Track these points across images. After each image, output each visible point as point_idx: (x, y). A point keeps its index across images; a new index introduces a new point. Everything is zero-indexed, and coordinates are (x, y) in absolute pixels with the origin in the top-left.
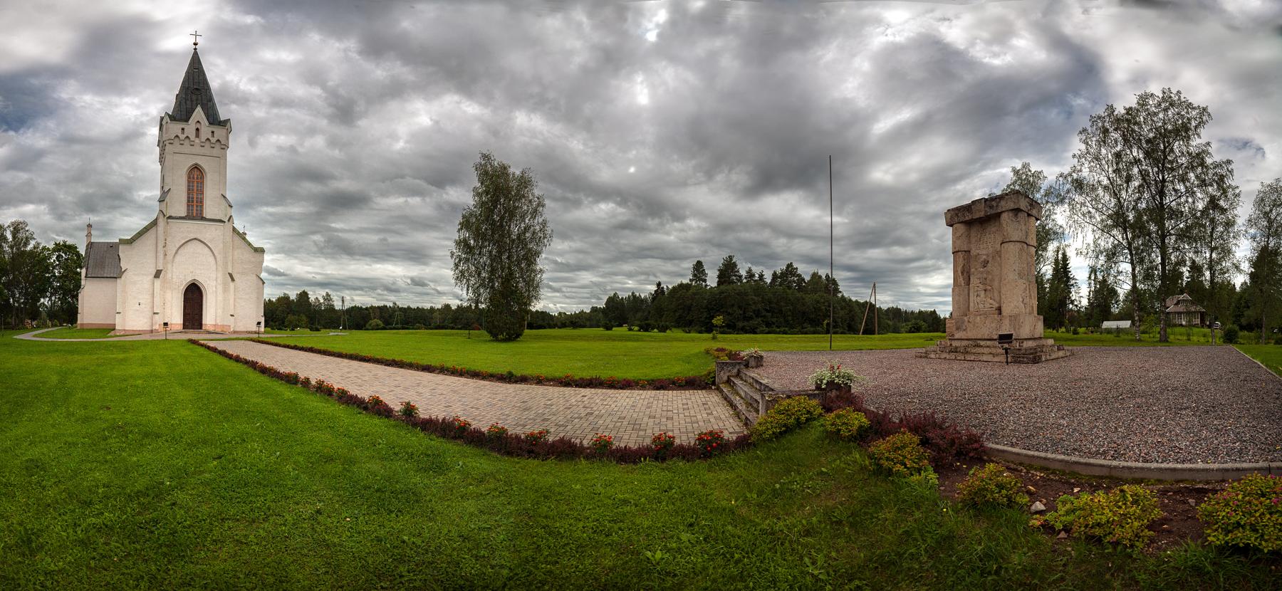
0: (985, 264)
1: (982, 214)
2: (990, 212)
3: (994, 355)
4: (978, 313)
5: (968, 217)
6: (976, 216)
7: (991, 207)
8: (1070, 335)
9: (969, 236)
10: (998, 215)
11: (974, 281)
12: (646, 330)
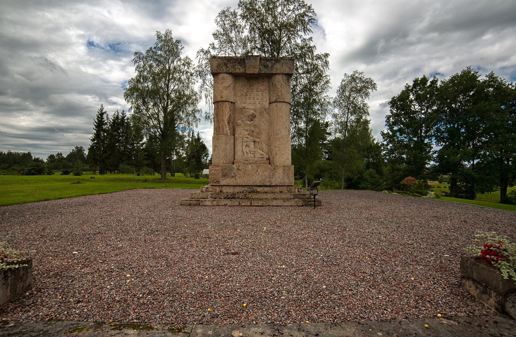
0: (252, 117)
1: (256, 71)
2: (264, 71)
3: (284, 200)
4: (247, 162)
5: (239, 70)
6: (250, 71)
7: (266, 67)
8: (193, 179)
9: (234, 89)
10: (270, 76)
11: (240, 132)
12: (50, 175)
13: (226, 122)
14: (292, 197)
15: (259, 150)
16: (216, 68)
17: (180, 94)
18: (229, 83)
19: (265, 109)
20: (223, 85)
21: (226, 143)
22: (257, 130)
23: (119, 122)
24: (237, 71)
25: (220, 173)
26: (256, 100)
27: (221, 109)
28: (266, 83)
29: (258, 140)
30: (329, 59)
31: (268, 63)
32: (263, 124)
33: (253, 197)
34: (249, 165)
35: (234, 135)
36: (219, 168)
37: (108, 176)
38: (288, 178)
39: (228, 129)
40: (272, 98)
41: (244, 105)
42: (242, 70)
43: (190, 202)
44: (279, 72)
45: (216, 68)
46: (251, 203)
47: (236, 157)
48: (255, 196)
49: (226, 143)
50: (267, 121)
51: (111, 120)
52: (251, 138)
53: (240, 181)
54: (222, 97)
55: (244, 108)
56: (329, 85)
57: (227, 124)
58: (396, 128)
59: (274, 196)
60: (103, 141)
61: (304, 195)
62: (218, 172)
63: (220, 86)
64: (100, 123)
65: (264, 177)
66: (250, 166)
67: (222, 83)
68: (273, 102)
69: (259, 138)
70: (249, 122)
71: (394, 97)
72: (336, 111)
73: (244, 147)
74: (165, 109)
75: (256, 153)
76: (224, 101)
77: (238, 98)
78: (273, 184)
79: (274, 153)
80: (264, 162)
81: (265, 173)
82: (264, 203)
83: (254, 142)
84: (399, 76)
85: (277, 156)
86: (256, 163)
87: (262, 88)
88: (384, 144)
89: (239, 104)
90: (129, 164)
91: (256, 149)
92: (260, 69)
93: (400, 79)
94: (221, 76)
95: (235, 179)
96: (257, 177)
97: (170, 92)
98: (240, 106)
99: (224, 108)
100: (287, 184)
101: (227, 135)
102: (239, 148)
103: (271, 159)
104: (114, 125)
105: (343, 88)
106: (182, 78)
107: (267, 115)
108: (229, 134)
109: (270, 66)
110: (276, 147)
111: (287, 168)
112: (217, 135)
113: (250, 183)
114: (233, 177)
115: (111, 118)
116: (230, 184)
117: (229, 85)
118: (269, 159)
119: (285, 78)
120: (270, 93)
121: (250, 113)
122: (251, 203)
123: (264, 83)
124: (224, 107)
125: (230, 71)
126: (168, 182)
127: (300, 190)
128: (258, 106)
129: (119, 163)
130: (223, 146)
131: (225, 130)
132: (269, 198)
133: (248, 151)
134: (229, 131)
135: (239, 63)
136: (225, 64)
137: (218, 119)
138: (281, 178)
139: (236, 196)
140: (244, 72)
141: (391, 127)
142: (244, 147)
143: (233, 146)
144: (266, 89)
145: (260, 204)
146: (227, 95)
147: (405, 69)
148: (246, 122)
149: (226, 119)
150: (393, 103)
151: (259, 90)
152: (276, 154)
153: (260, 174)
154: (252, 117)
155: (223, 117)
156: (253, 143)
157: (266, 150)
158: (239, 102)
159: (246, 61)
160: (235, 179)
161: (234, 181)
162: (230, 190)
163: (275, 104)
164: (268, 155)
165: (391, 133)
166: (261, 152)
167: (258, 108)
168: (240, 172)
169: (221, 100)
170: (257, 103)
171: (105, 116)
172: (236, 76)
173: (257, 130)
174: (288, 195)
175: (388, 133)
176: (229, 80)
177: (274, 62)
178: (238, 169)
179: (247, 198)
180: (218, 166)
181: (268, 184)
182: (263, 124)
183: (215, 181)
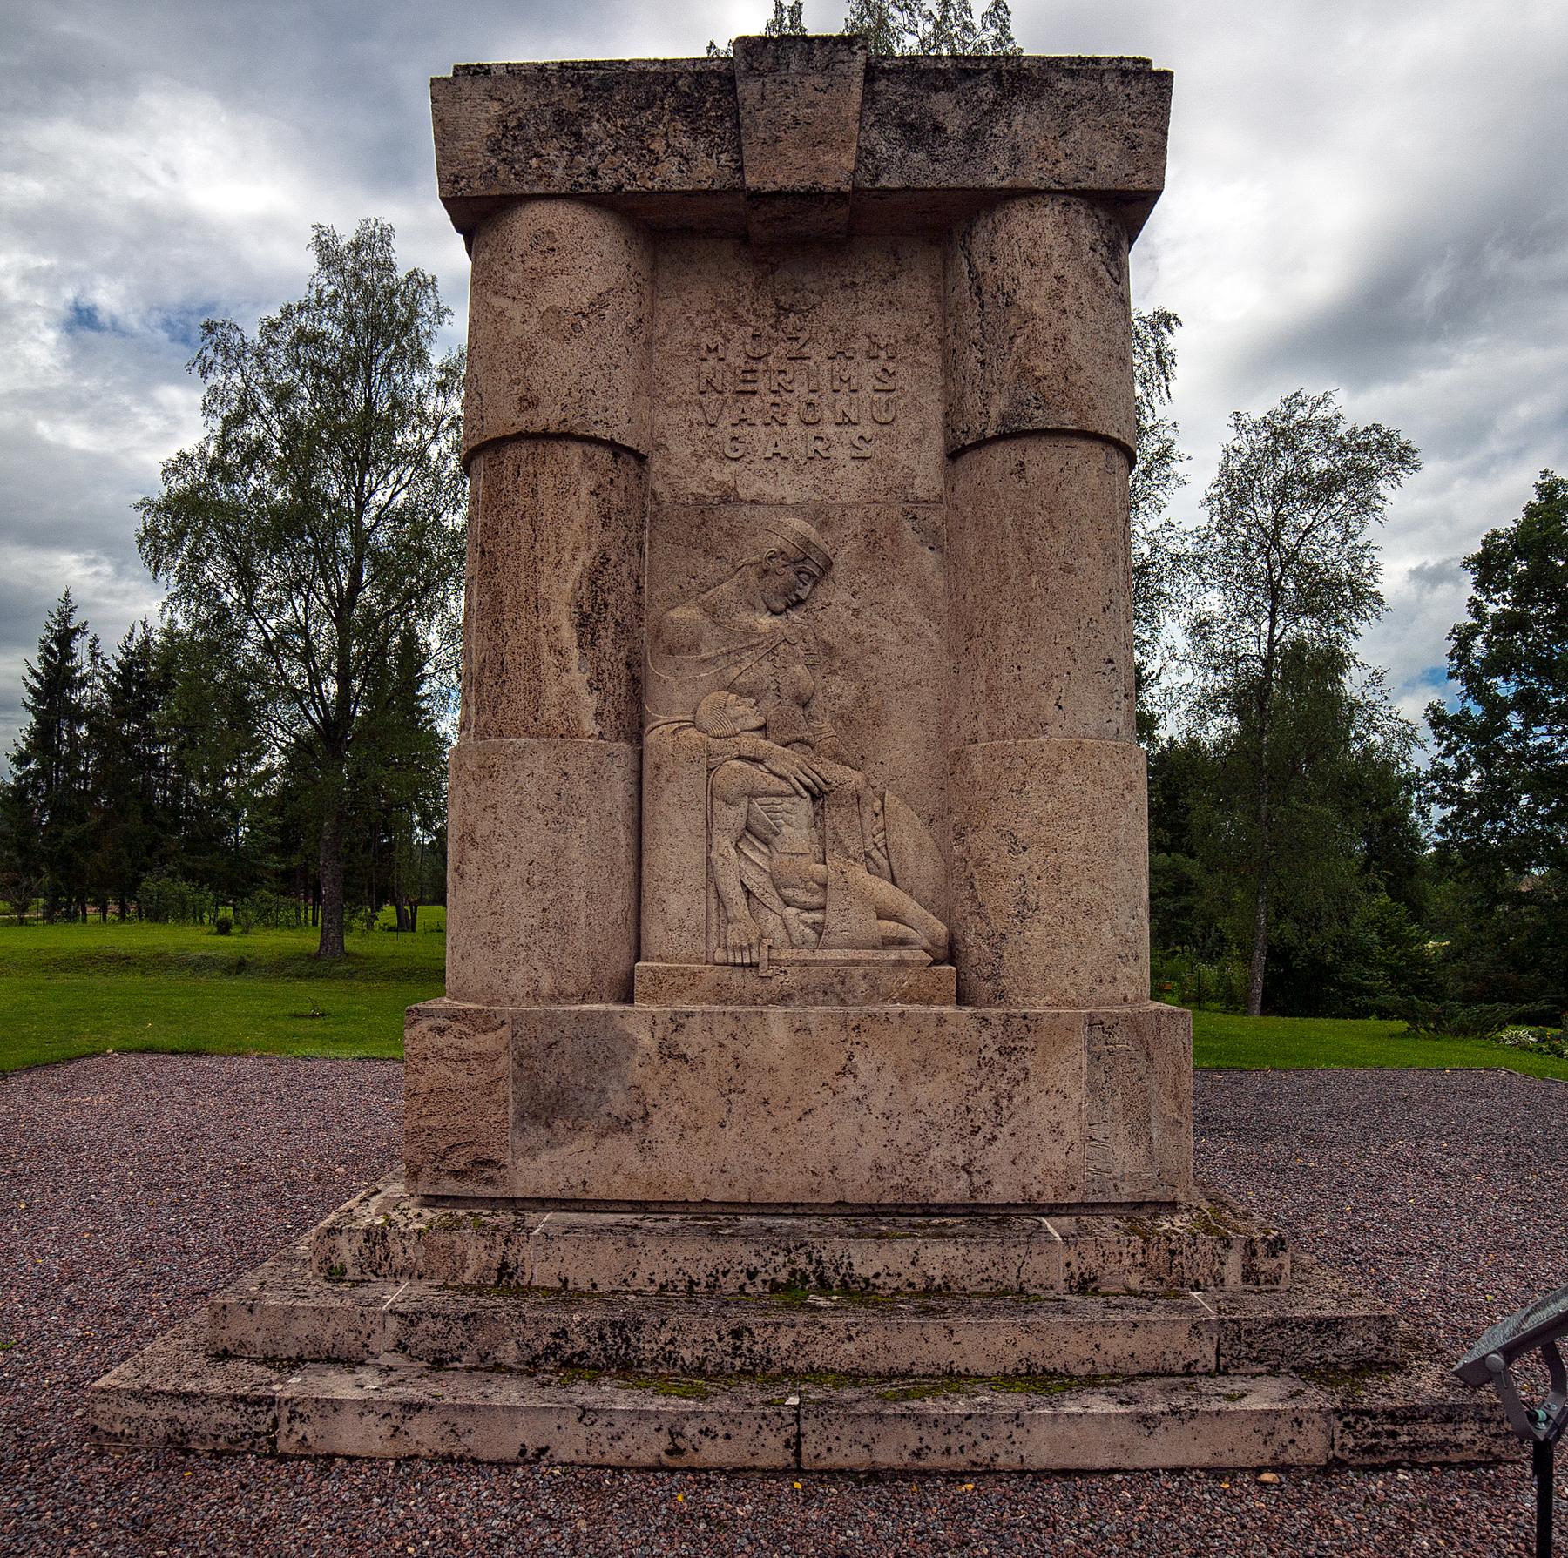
0: (799, 577)
1: (837, 168)
2: (904, 169)
4: (749, 982)
5: (685, 165)
6: (779, 169)
7: (920, 133)
9: (643, 334)
11: (687, 703)
13: (563, 618)
14: (1205, 1353)
15: (859, 873)
16: (484, 160)
17: (419, 533)
18: (598, 284)
19: (913, 507)
20: (543, 300)
21: (562, 812)
22: (843, 689)
23: (147, 675)
24: (669, 175)
25: (506, 1090)
26: (829, 430)
27: (522, 501)
28: (915, 289)
29: (849, 778)
30: (1174, 341)
31: (941, 103)
32: (890, 637)
33: (820, 1353)
34: (775, 1012)
35: (635, 732)
36: (488, 1042)
37: (97, 933)
38: (1139, 1132)
39: (578, 679)
40: (972, 402)
41: (724, 474)
42: (708, 170)
43: (180, 1411)
44: (1032, 180)
45: (484, 160)
46: (795, 1444)
47: (655, 933)
48: (835, 1339)
49: (562, 812)
50: (928, 609)
51: (112, 664)
52: (789, 761)
53: (684, 1162)
54: (528, 403)
55: (728, 497)
56: (1176, 468)
57: (568, 634)
58: (1505, 688)
59: (1027, 1344)
60: (70, 762)
61: (1322, 1325)
62: (481, 1076)
63: (516, 311)
64: (56, 679)
65: (913, 1125)
66: (778, 1022)
67: (537, 278)
68: (983, 443)
69: (859, 763)
70: (765, 621)
71: (1495, 534)
72: (1213, 602)
73: (724, 843)
74: (343, 606)
75: (836, 900)
76: (545, 436)
77: (676, 416)
78: (1002, 1191)
79: (1000, 896)
80: (908, 978)
81: (924, 1092)
82: (936, 1440)
83: (817, 796)
84: (1495, 446)
85: (1036, 932)
86: (834, 989)
87: (883, 325)
88: (1445, 770)
89: (685, 468)
90: (189, 874)
91: (836, 861)
92: (866, 153)
93: (1492, 459)
94: (527, 222)
95: (646, 1148)
96: (847, 1128)
97: (367, 520)
98: (694, 486)
99: (546, 497)
100: (1127, 1192)
101: (572, 734)
102: (676, 849)
103: (976, 950)
104: (127, 692)
105: (1236, 489)
106: (433, 451)
107: (929, 559)
108: (590, 726)
109: (954, 124)
110: (1018, 847)
111: (1123, 1041)
112: (484, 733)
113: (784, 1183)
114: (623, 1125)
115: (113, 653)
116: (598, 1190)
117: (598, 303)
118: (951, 952)
119: (1087, 233)
120: (950, 357)
121: (777, 542)
122: (795, 1444)
123: (903, 287)
124: (547, 483)
125: (606, 182)
126: (351, 975)
127: (1265, 1264)
128: (851, 480)
129: (146, 869)
130: (535, 836)
131: (552, 691)
132: (976, 1363)
133: (758, 882)
134: (591, 701)
135: (687, 109)
136: (567, 124)
137: (496, 598)
138: (1072, 1132)
139: (649, 1345)
140: (726, 179)
141: (1475, 685)
142: (724, 843)
143: (623, 836)
144: (914, 340)
145: (886, 1456)
146: (586, 377)
147: (1524, 411)
148: (745, 618)
149: (561, 592)
150: (1489, 565)
151: (861, 344)
152: (1025, 910)
153: (879, 1102)
154: (799, 577)
155: (535, 575)
156: (803, 808)
157: (924, 867)
158: (680, 450)
159: (748, 90)
160: (646, 1148)
161: (633, 1161)
162: (592, 1263)
163: (999, 458)
164: (946, 916)
165: (1476, 711)
166: (883, 890)
167: (848, 495)
168: (686, 1080)
169: (521, 422)
170: (842, 454)
171: (80, 646)
172: (663, 229)
173: (843, 689)
174: (1162, 1334)
175: (1466, 713)
176: (588, 257)
177: (987, 92)
178: (670, 1053)
179: (761, 1370)
180: (484, 1023)
181: (953, 1190)
182: (890, 637)
183: (459, 1161)
